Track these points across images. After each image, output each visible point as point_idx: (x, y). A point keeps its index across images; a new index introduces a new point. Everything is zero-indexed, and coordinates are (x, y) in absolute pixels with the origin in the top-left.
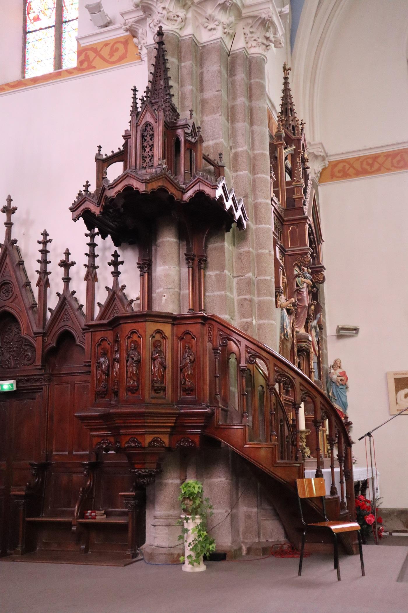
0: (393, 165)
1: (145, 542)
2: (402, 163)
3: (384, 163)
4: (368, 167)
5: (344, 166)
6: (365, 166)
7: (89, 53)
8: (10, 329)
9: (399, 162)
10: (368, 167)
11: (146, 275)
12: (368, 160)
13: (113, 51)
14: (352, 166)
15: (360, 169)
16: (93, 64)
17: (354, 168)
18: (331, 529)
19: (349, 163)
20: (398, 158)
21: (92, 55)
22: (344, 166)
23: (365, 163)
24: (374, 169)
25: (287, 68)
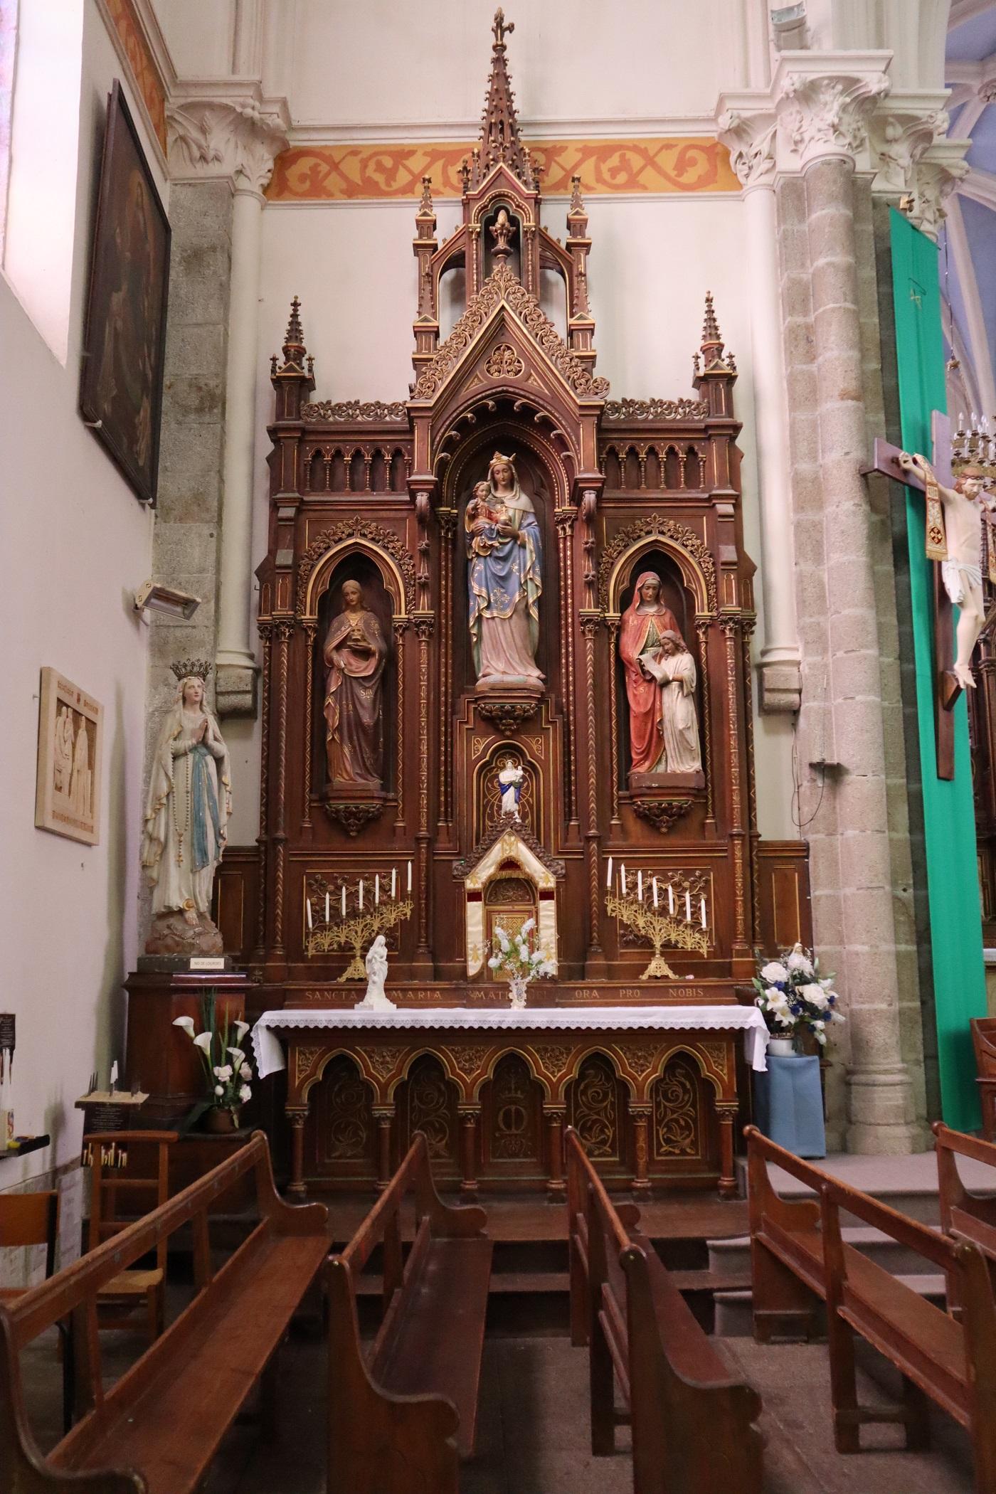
0: (600, 179)
1: (352, 1007)
2: (622, 178)
3: (575, 167)
4: (380, 178)
5: (317, 165)
6: (370, 172)
8: (646, 1058)
9: (614, 172)
10: (380, 178)
11: (941, 668)
15: (357, 179)
16: (642, 179)
18: (828, 1292)
19: (328, 159)
20: (614, 161)
21: (636, 161)
22: (317, 165)
23: (372, 165)
24: (395, 186)
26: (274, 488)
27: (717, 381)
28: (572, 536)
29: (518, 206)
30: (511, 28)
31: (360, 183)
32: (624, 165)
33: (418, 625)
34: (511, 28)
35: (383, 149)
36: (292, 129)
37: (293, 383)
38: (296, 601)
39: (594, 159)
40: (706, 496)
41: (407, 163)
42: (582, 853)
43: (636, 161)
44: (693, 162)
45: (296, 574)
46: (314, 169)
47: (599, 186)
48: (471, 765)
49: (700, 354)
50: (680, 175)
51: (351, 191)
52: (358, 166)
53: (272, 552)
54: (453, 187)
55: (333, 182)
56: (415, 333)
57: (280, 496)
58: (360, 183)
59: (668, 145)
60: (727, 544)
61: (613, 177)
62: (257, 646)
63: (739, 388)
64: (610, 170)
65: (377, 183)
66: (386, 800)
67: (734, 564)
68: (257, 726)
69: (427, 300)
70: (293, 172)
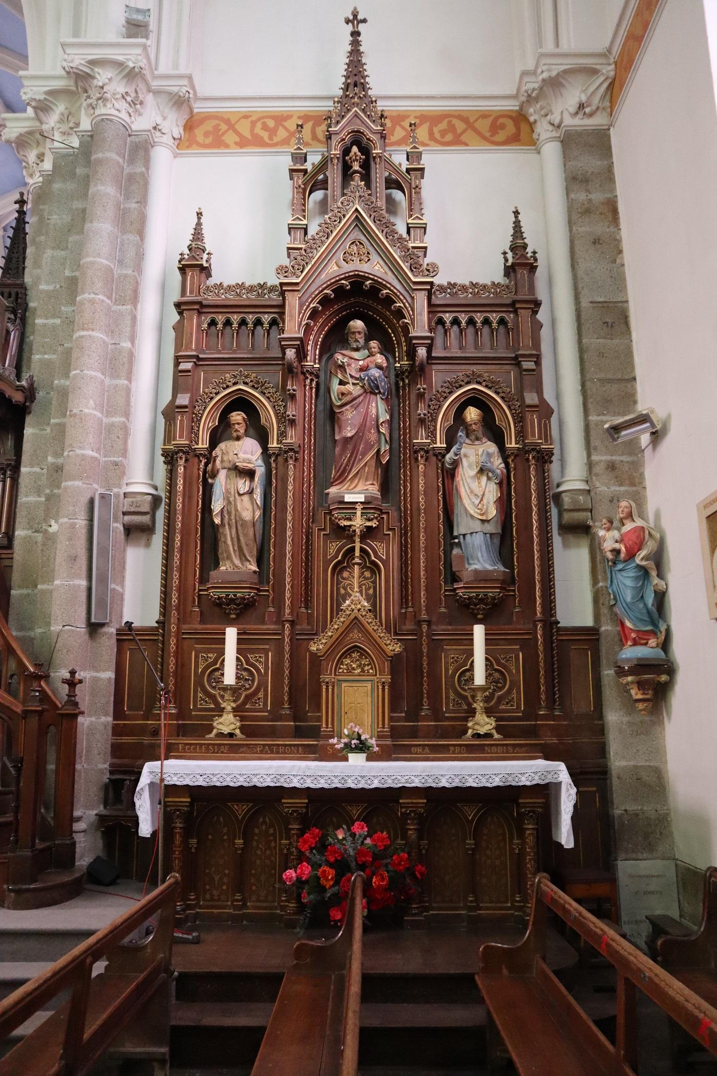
2: (449, 137)
4: (265, 135)
5: (219, 125)
6: (258, 129)
7: (455, 121)
10: (265, 135)
12: (266, 120)
13: (495, 127)
14: (231, 126)
15: (247, 134)
16: (463, 138)
17: (237, 132)
19: (227, 121)
20: (443, 125)
23: (259, 125)
25: (360, 17)
26: (178, 345)
27: (521, 263)
28: (409, 384)
29: (368, 139)
30: (364, 21)
31: (250, 137)
32: (452, 128)
33: (286, 452)
34: (364, 21)
35: (266, 114)
36: (197, 98)
37: (194, 266)
38: (193, 433)
39: (428, 124)
40: (513, 355)
41: (286, 124)
42: (415, 634)
43: (460, 126)
44: (503, 127)
45: (192, 413)
46: (216, 128)
47: (432, 143)
48: (327, 563)
49: (509, 251)
50: (492, 136)
51: (243, 143)
52: (249, 125)
53: (174, 396)
54: (319, 141)
55: (230, 138)
56: (290, 229)
57: (180, 354)
58: (250, 137)
59: (484, 115)
60: (531, 392)
61: (443, 136)
62: (161, 469)
63: (540, 273)
64: (440, 132)
65: (262, 138)
66: (258, 590)
67: (536, 406)
68: (158, 539)
69: (301, 207)
70: (199, 133)
